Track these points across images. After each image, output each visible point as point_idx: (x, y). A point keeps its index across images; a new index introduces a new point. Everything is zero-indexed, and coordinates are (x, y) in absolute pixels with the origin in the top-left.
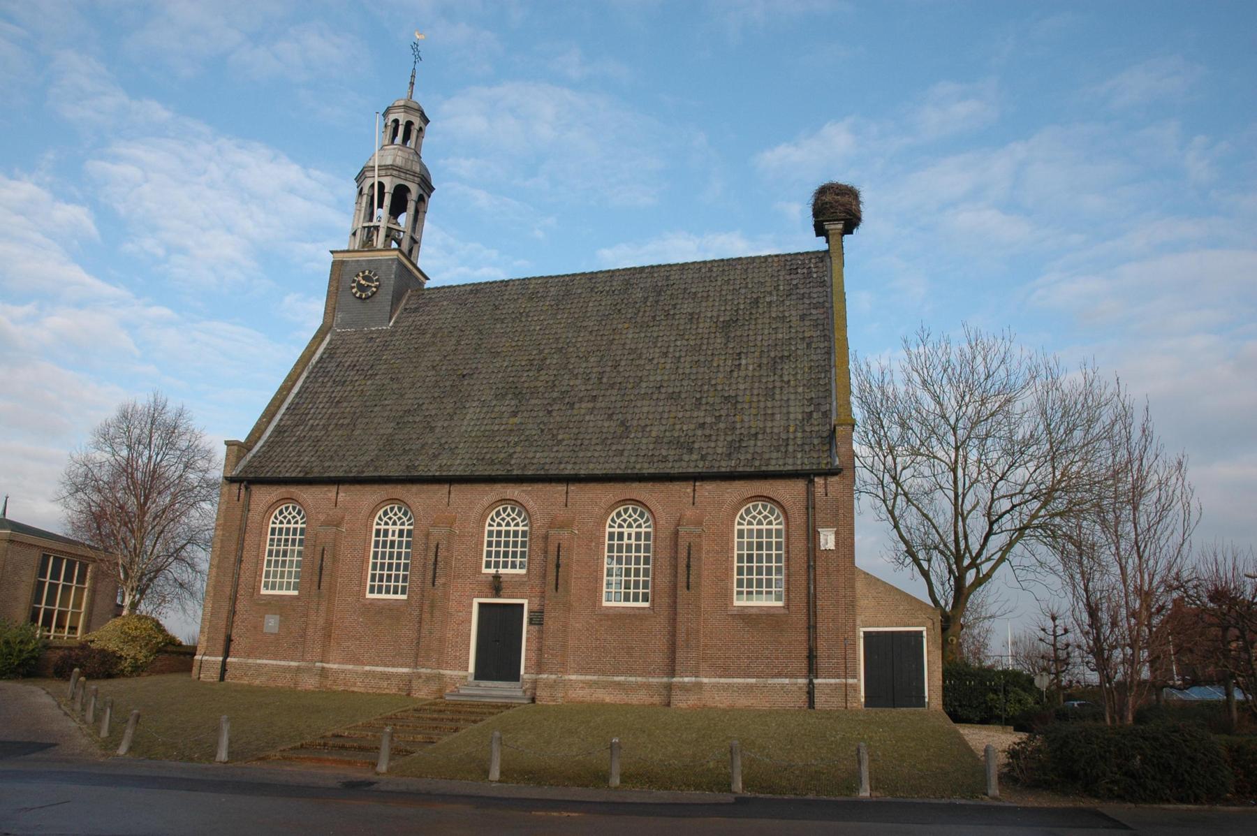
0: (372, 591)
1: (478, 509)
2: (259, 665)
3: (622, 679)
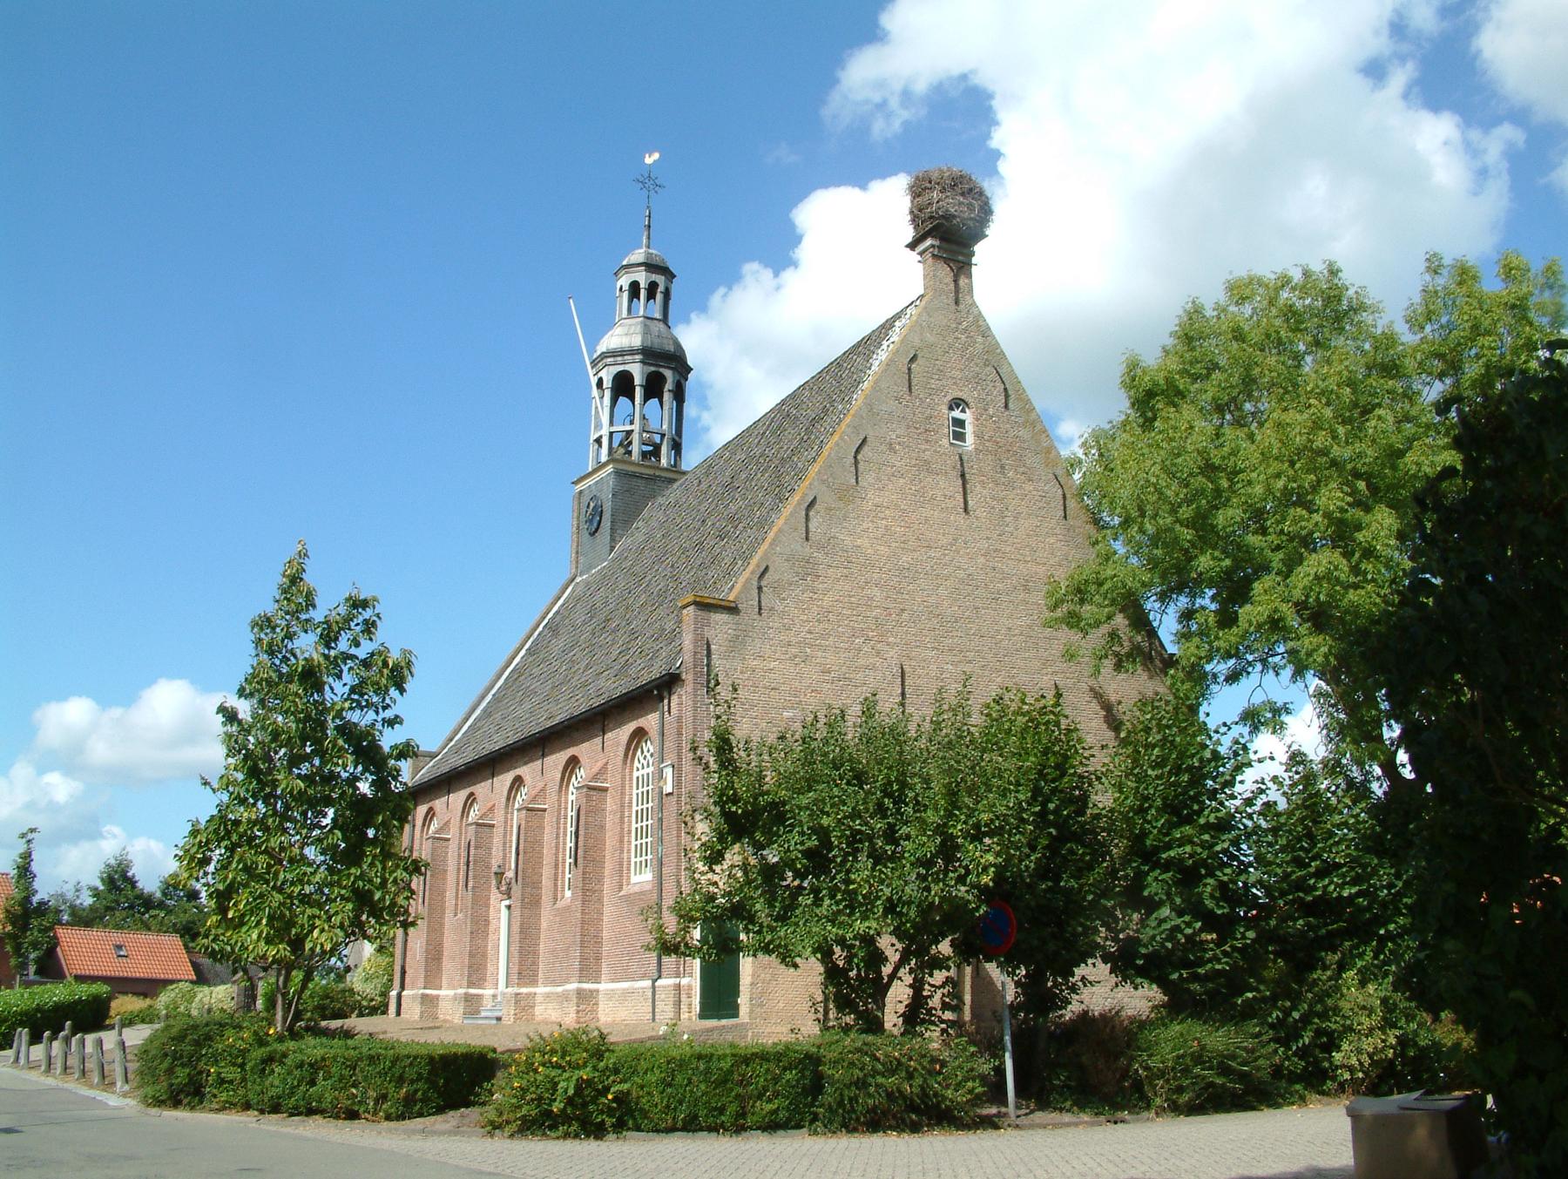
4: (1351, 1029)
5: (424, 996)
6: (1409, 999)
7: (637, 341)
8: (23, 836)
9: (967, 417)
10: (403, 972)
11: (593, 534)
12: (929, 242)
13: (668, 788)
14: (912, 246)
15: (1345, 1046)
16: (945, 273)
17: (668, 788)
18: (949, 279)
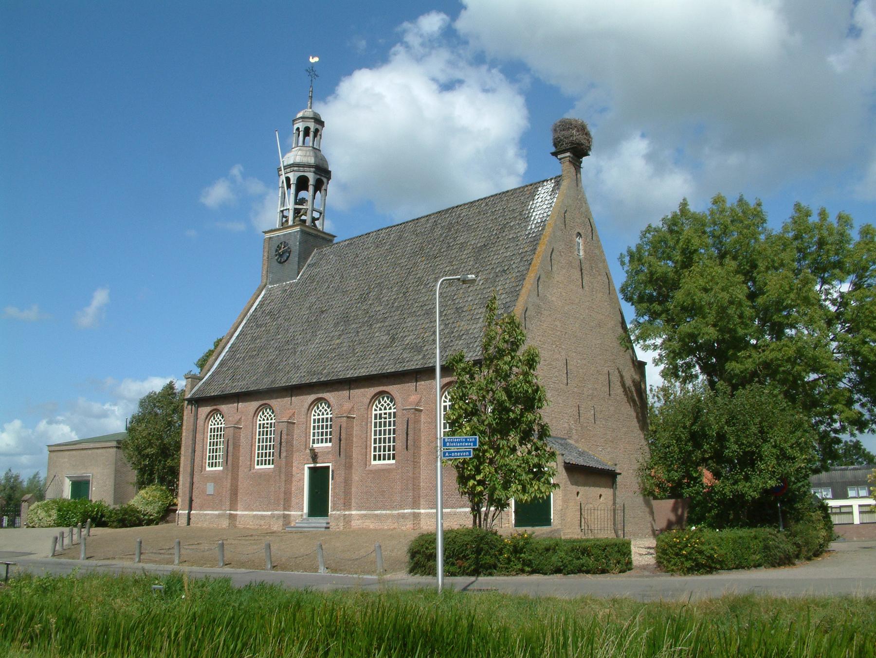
0: (375, 459)
1: (306, 406)
2: (206, 514)
3: (379, 512)
12: (568, 154)
14: (555, 154)
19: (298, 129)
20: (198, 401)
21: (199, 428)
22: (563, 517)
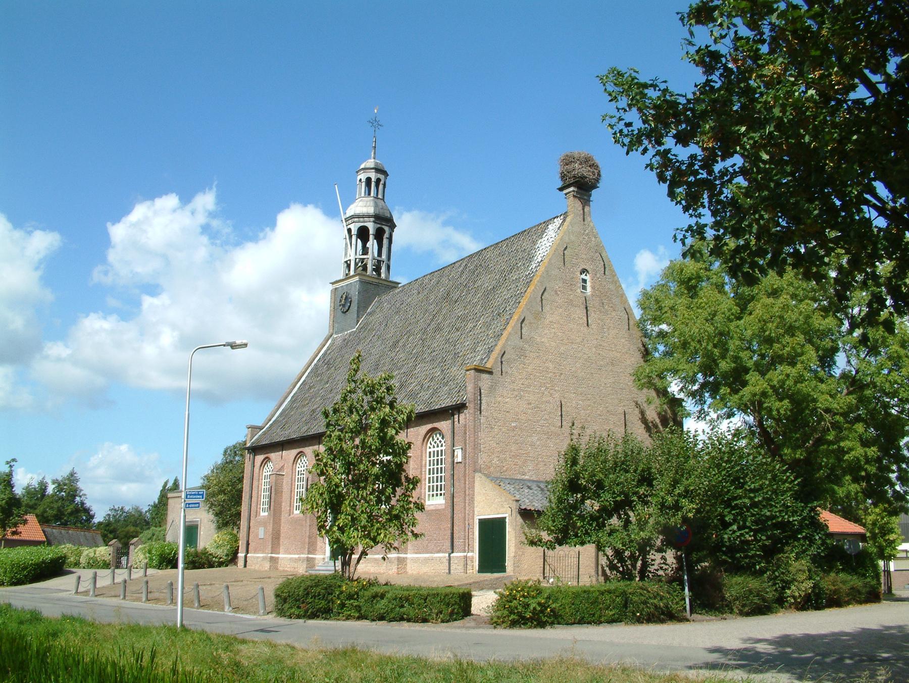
4: (794, 580)
5: (272, 558)
6: (816, 567)
7: (371, 210)
8: (8, 463)
9: (588, 278)
10: (248, 544)
11: (344, 313)
12: (572, 189)
13: (459, 459)
15: (793, 587)
16: (578, 204)
17: (459, 459)
18: (580, 208)
19: (360, 180)
20: (255, 450)
21: (256, 475)
22: (516, 566)
